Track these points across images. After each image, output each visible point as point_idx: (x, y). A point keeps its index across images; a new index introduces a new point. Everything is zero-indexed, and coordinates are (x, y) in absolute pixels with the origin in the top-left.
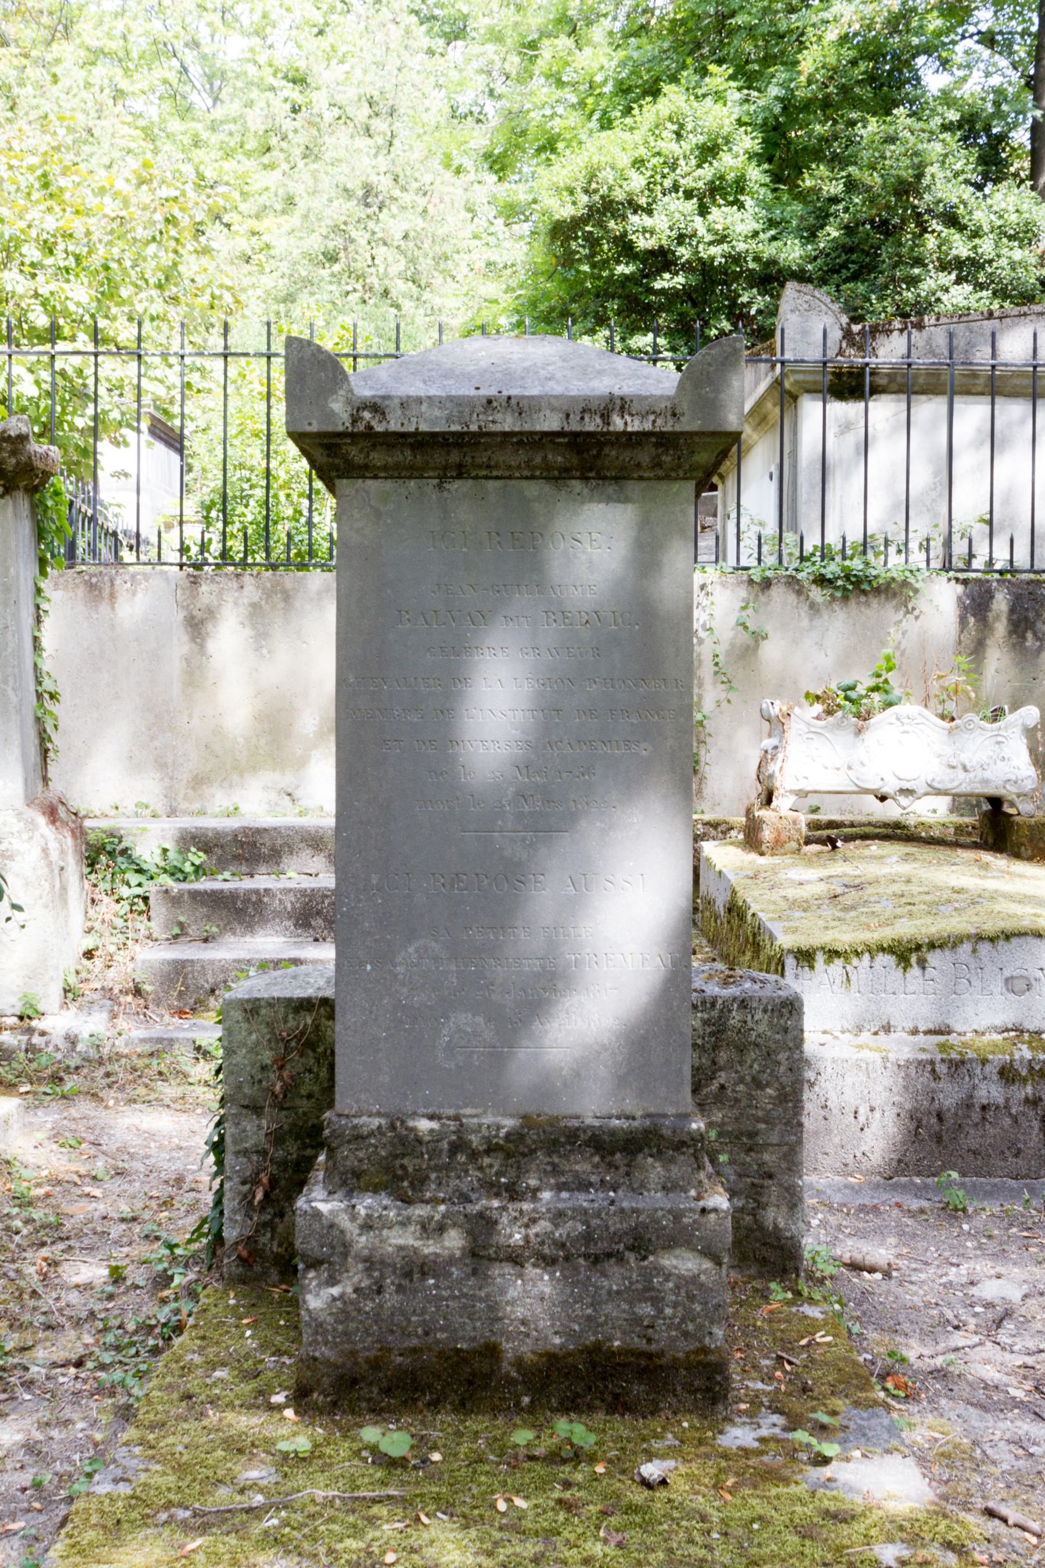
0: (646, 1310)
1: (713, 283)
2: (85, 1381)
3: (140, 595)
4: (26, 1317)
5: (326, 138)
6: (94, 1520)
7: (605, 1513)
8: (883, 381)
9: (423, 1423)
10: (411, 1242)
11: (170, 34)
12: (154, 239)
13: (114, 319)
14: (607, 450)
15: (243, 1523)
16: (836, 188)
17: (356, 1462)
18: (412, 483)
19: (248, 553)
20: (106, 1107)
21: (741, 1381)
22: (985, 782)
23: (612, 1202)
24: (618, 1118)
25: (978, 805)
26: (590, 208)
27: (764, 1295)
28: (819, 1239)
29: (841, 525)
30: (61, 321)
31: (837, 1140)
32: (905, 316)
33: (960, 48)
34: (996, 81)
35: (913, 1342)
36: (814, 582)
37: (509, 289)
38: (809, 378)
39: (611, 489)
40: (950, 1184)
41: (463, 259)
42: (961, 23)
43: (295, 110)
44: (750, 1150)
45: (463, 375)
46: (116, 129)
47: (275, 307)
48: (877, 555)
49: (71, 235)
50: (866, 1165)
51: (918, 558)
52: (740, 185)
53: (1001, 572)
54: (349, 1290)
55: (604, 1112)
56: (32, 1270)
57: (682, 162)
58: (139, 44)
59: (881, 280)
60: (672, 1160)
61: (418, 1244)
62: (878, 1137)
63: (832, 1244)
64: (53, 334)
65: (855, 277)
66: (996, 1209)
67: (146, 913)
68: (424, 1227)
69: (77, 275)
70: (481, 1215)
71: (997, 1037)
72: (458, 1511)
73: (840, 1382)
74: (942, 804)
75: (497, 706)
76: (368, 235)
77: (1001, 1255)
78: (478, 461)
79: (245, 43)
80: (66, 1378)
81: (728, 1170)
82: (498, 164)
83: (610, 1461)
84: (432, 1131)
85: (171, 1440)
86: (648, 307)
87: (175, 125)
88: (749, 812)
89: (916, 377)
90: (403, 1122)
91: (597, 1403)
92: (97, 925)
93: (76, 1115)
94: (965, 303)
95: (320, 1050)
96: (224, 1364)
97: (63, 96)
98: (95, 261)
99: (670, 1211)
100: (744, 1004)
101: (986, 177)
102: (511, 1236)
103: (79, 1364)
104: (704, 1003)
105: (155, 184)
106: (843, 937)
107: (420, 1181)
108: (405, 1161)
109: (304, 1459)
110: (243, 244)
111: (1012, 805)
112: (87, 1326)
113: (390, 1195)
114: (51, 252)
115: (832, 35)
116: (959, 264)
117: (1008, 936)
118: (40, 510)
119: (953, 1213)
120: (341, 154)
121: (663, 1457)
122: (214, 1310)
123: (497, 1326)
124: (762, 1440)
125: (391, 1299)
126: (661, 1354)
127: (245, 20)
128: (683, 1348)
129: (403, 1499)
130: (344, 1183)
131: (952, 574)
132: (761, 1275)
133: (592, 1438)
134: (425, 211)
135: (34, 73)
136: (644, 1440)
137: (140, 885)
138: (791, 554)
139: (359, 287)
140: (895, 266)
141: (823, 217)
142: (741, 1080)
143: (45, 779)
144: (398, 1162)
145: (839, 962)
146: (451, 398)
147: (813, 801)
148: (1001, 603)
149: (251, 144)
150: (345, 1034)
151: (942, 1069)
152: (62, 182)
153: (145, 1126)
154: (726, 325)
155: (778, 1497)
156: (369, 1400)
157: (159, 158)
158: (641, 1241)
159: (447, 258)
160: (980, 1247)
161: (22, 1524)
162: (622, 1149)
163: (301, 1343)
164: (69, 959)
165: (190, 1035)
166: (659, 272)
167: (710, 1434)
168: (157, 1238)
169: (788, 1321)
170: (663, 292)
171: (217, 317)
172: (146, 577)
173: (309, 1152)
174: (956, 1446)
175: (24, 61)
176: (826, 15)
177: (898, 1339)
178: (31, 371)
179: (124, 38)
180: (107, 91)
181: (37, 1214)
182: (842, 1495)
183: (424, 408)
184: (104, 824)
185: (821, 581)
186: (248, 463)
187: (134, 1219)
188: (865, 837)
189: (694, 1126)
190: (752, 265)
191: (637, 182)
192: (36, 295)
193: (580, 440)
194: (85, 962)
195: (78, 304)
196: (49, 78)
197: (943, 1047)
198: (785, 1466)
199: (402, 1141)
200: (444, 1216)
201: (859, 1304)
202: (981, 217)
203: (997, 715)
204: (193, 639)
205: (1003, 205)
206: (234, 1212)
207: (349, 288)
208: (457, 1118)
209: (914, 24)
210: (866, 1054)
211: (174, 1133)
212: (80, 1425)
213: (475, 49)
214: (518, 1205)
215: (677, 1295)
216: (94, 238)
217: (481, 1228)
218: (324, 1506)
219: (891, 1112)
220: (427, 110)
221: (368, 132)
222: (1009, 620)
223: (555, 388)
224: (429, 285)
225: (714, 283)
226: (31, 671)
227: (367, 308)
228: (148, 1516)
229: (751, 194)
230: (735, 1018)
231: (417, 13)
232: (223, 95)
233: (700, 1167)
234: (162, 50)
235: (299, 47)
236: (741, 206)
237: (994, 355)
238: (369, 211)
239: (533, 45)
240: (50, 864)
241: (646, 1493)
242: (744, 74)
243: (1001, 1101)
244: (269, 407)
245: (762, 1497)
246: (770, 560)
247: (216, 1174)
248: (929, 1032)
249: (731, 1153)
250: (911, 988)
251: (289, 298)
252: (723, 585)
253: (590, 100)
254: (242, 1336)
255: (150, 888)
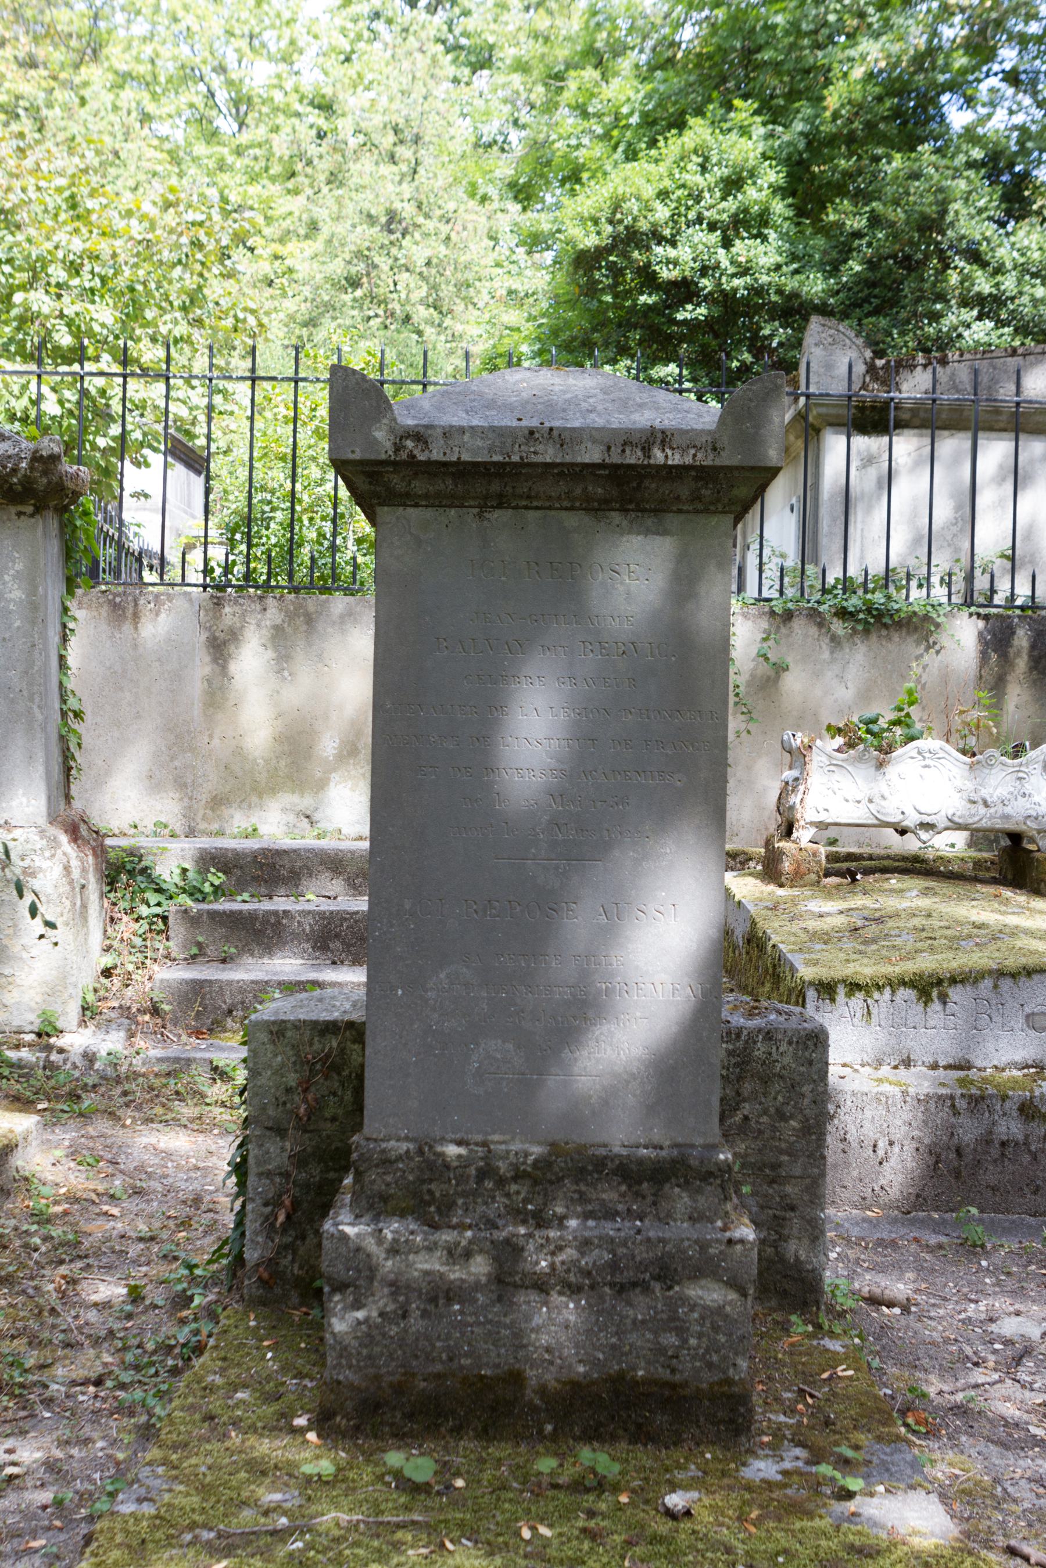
0: (670, 1340)
1: (735, 313)
2: (104, 1400)
3: (163, 616)
4: (45, 1335)
5: (351, 164)
6: (119, 1539)
7: (629, 1543)
8: (906, 416)
9: (445, 1448)
10: (437, 1267)
11: (198, 60)
12: (180, 262)
13: (138, 340)
14: (647, 483)
15: (267, 1545)
16: (858, 223)
17: (379, 1487)
18: (453, 512)
19: (269, 575)
20: (124, 1126)
21: (764, 1413)
22: (1006, 817)
23: (639, 1232)
24: (646, 1147)
25: (997, 840)
26: (614, 238)
27: (785, 1328)
28: (840, 1272)
29: (862, 558)
30: (86, 342)
31: (855, 1173)
32: (927, 351)
33: (984, 87)
34: (1019, 119)
35: (933, 1378)
36: (836, 614)
37: (531, 318)
38: (833, 411)
39: (649, 522)
40: (970, 1219)
41: (484, 287)
42: (986, 62)
43: (321, 136)
44: (772, 1182)
45: (505, 405)
46: (143, 152)
47: (297, 332)
48: (898, 589)
49: (97, 257)
50: (884, 1199)
51: (939, 593)
52: (763, 219)
53: (1022, 608)
54: (375, 1314)
55: (632, 1140)
56: (51, 1287)
57: (707, 195)
58: (167, 68)
59: (903, 315)
60: (699, 1191)
61: (444, 1269)
62: (896, 1171)
63: (850, 1278)
64: (78, 354)
65: (877, 312)
66: (1015, 1246)
67: (165, 932)
68: (450, 1253)
69: (102, 297)
70: (507, 1241)
71: (1016, 1073)
72: (483, 1537)
73: (863, 1416)
74: (960, 838)
75: (535, 732)
76: (390, 261)
77: (1019, 1293)
78: (519, 491)
79: (272, 68)
80: (86, 1396)
81: (751, 1202)
82: (523, 193)
83: (633, 1491)
84: (460, 1156)
85: (193, 1461)
86: (670, 337)
87: (200, 149)
88: (768, 843)
89: (939, 412)
90: (431, 1147)
91: (620, 1432)
92: (116, 944)
93: (94, 1133)
94: (986, 339)
95: (345, 1073)
96: (245, 1386)
97: (90, 118)
98: (121, 282)
99: (696, 1242)
100: (769, 1035)
101: (1009, 213)
102: (537, 1263)
103: (98, 1382)
104: (729, 1033)
105: (181, 208)
106: (865, 970)
107: (446, 1207)
108: (433, 1186)
109: (327, 1483)
110: (265, 268)
111: (1032, 840)
112: (106, 1345)
113: (417, 1219)
114: (78, 273)
115: (858, 73)
116: (980, 300)
117: (1029, 972)
118: (68, 530)
119: (972, 1249)
120: (366, 180)
121: (686, 1488)
122: (235, 1332)
123: (521, 1354)
124: (785, 1473)
125: (416, 1323)
126: (685, 1384)
127: (273, 48)
128: (708, 1378)
129: (427, 1525)
130: (371, 1207)
131: (973, 609)
132: (781, 1308)
133: (616, 1468)
134: (448, 238)
135: (61, 95)
136: (667, 1470)
137: (159, 904)
138: (811, 586)
139: (381, 312)
140: (918, 300)
141: (846, 251)
142: (765, 1112)
143: (68, 798)
144: (425, 1187)
145: (860, 995)
146: (493, 429)
147: (832, 833)
148: (1022, 638)
149: (276, 169)
150: (378, 1060)
151: (961, 1104)
152: (90, 204)
153: (162, 1145)
154: (747, 357)
155: (802, 1531)
156: (392, 1425)
157: (184, 181)
158: (667, 1271)
159: (468, 286)
160: (998, 1283)
161: (43, 1542)
162: (649, 1178)
163: (324, 1365)
164: (86, 977)
165: (207, 1055)
166: (681, 303)
167: (733, 1466)
168: (176, 1258)
169: (810, 1355)
170: (685, 322)
171: (241, 341)
172: (170, 598)
173: (332, 1175)
174: (977, 1483)
175: (52, 83)
176: (852, 53)
177: (918, 1374)
178: (54, 390)
179: (152, 62)
180: (134, 114)
181: (56, 1232)
182: (866, 1530)
183: (466, 437)
184: (124, 842)
185: (843, 613)
186: (270, 485)
187: (152, 1239)
188: (884, 870)
189: (722, 1157)
190: (774, 298)
191: (662, 213)
192: (61, 316)
193: (621, 472)
194: (103, 980)
195: (103, 325)
196: (77, 100)
197: (963, 1082)
198: (809, 1499)
199: (430, 1166)
200: (470, 1242)
201: (878, 1339)
202: (1004, 254)
203: (1018, 751)
204: (215, 661)
205: (1026, 242)
206: (256, 1233)
207: (371, 313)
208: (485, 1144)
209: (940, 62)
210: (886, 1088)
211: (195, 1152)
212: (100, 1444)
213: (500, 79)
214: (544, 1232)
215: (702, 1325)
216: (121, 259)
217: (508, 1254)
218: (348, 1530)
219: (909, 1147)
220: (452, 138)
221: (392, 159)
222: (1030, 656)
223: (598, 421)
224: (451, 311)
225: (737, 314)
226: (56, 689)
227: (389, 333)
228: (172, 1536)
229: (775, 227)
230: (760, 1050)
231: (443, 42)
232: (249, 120)
233: (727, 1198)
234: (188, 75)
235: (326, 74)
236: (765, 239)
237: (1018, 393)
238: (393, 237)
239: (559, 77)
240: (71, 882)
241: (670, 1524)
242: (770, 109)
243: (1020, 1137)
244: (295, 431)
245: (786, 1531)
246: (790, 592)
247: (237, 1196)
248: (948, 1067)
249: (753, 1184)
250: (932, 1023)
251: (311, 323)
252: (745, 616)
253: (615, 133)
254: (263, 1357)
255: (170, 908)
